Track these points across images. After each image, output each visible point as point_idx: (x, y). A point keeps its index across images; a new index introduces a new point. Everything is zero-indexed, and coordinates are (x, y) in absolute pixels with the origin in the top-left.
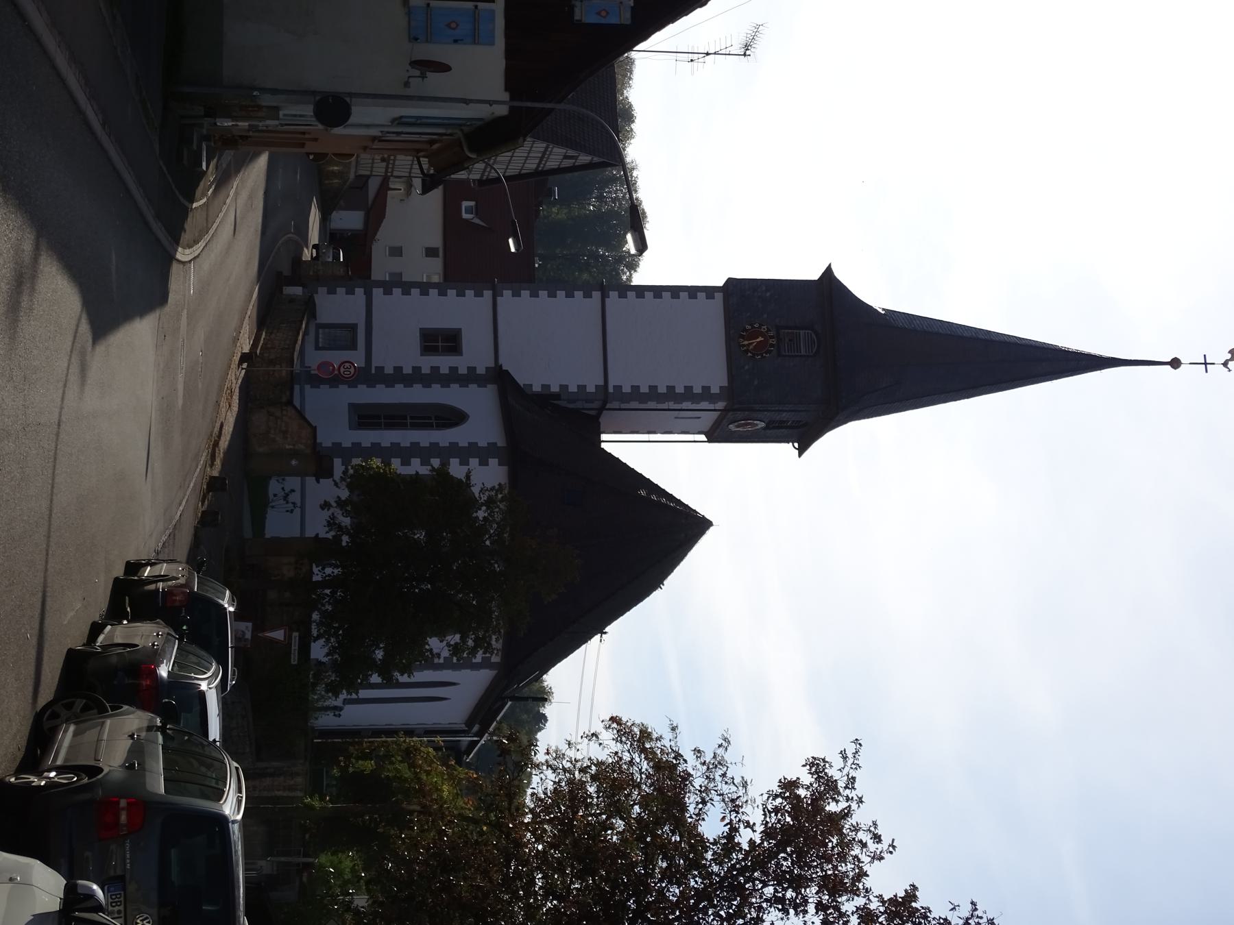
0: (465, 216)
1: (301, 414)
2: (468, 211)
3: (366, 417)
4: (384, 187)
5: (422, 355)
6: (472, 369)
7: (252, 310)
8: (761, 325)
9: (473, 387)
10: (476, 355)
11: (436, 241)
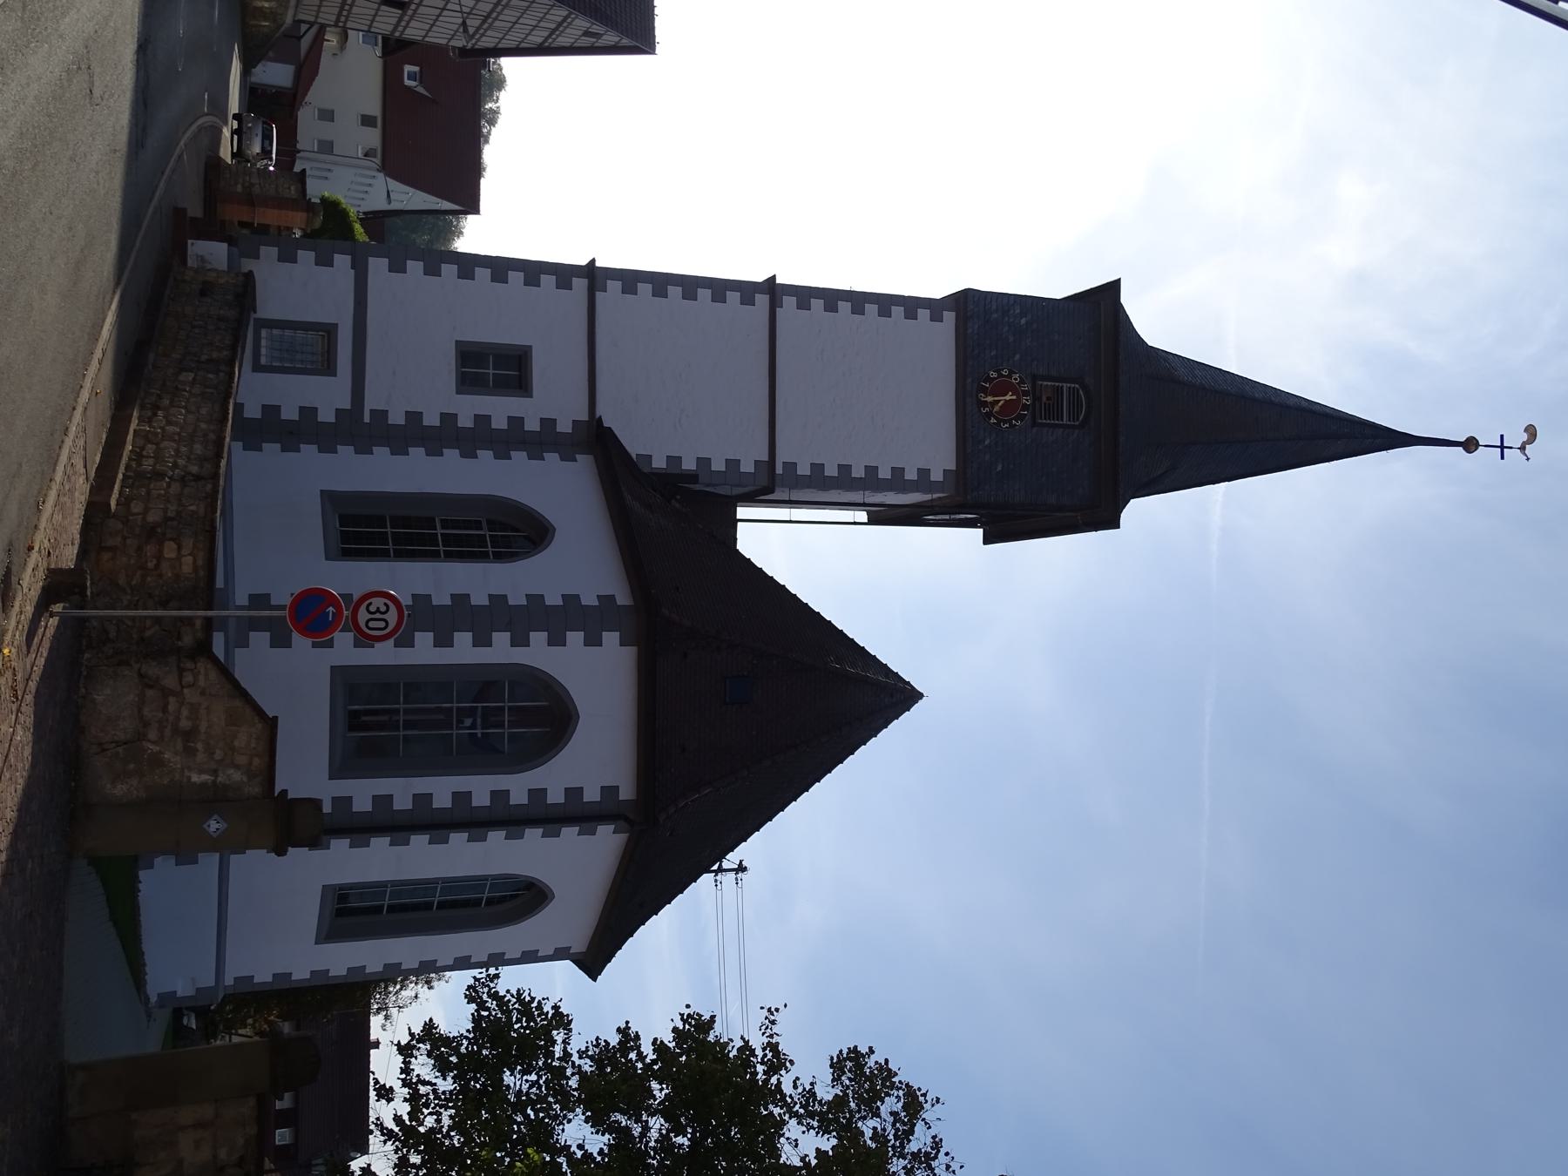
0: (407, 82)
1: (225, 672)
2: (412, 76)
3: (363, 528)
4: (319, 40)
5: (458, 392)
6: (548, 423)
7: (98, 376)
8: (1011, 372)
11: (375, 109)
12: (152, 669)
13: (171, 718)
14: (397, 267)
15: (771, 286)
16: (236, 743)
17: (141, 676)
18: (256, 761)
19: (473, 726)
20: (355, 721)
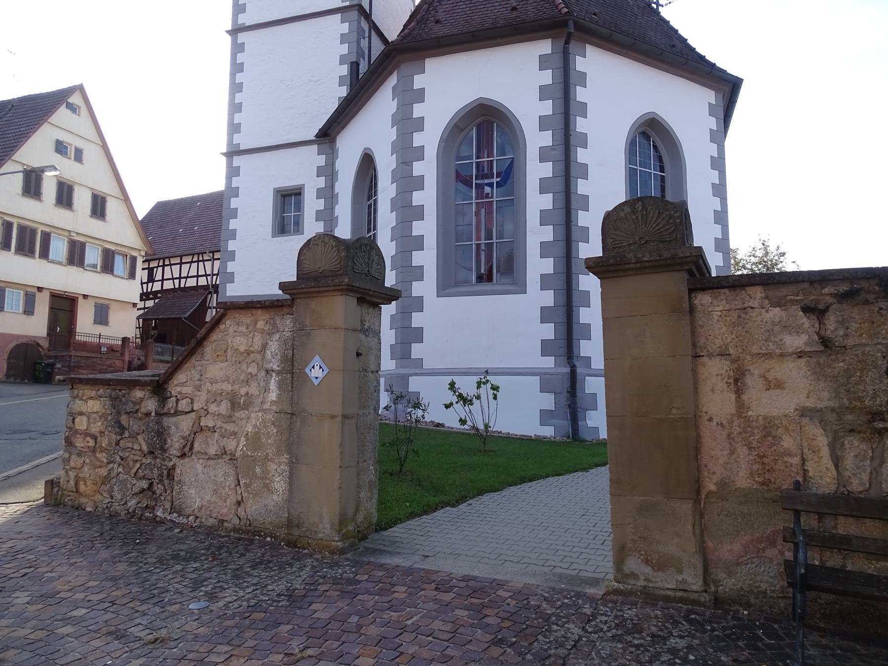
12: (175, 444)
13: (219, 424)
14: (231, 278)
16: (242, 349)
17: (183, 456)
18: (261, 324)
19: (491, 185)
20: (485, 278)
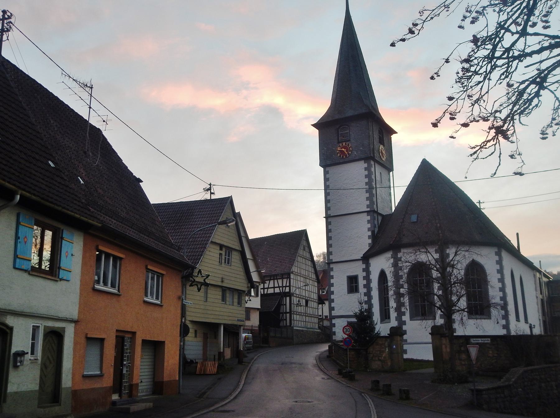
6: (364, 270)
9: (371, 269)
10: (357, 269)
15: (327, 217)
